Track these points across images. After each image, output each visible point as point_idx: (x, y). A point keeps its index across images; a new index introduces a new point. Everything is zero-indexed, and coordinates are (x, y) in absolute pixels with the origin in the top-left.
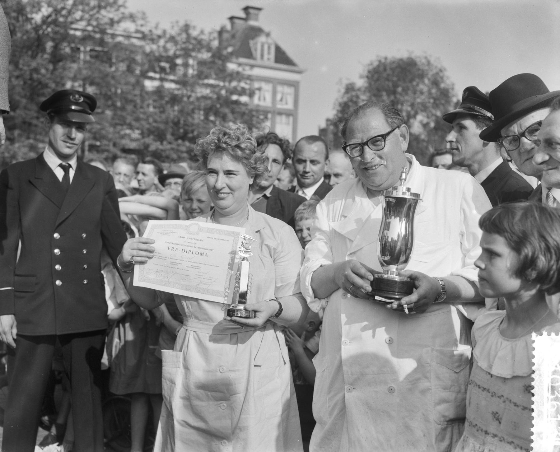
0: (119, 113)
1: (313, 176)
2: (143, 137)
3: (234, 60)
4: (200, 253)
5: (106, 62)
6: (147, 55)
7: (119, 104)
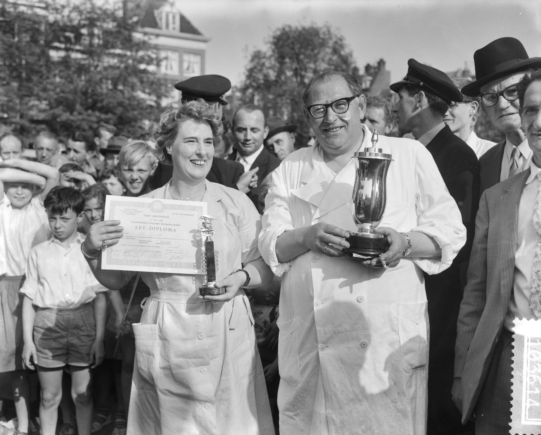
0: (25, 83)
1: (254, 143)
2: (51, 108)
3: (140, 29)
4: (168, 229)
5: (8, 32)
6: (51, 25)
7: (24, 75)
